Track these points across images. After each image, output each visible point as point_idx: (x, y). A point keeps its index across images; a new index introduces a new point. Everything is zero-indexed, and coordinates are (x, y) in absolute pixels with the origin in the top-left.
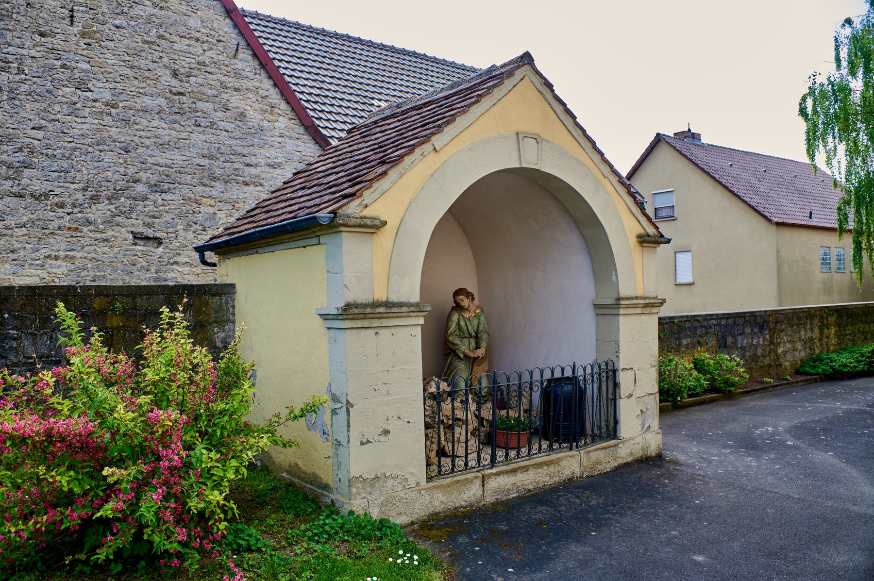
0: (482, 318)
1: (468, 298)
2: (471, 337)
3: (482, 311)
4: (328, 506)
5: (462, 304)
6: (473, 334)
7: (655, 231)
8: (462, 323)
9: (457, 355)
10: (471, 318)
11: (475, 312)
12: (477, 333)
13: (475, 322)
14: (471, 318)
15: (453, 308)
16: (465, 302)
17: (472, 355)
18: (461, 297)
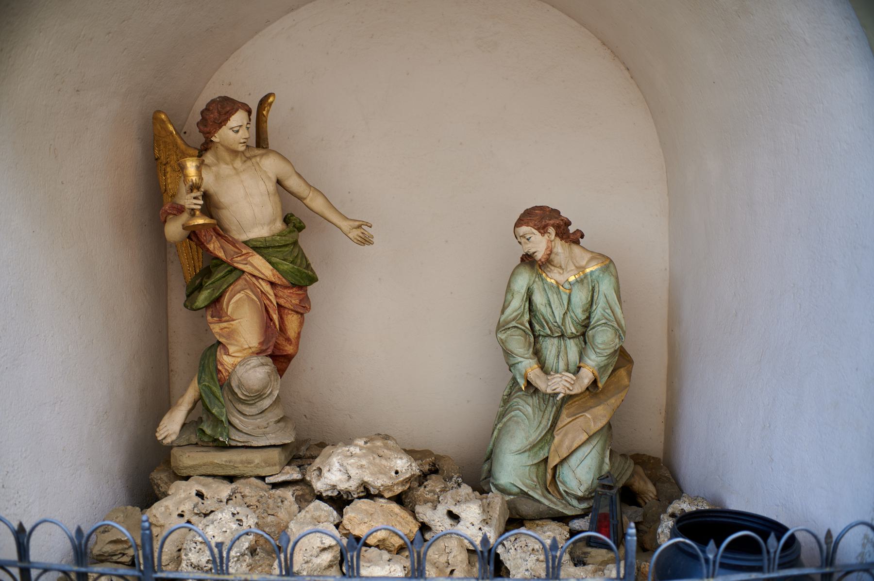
0: (606, 287)
8: (539, 299)
13: (580, 297)
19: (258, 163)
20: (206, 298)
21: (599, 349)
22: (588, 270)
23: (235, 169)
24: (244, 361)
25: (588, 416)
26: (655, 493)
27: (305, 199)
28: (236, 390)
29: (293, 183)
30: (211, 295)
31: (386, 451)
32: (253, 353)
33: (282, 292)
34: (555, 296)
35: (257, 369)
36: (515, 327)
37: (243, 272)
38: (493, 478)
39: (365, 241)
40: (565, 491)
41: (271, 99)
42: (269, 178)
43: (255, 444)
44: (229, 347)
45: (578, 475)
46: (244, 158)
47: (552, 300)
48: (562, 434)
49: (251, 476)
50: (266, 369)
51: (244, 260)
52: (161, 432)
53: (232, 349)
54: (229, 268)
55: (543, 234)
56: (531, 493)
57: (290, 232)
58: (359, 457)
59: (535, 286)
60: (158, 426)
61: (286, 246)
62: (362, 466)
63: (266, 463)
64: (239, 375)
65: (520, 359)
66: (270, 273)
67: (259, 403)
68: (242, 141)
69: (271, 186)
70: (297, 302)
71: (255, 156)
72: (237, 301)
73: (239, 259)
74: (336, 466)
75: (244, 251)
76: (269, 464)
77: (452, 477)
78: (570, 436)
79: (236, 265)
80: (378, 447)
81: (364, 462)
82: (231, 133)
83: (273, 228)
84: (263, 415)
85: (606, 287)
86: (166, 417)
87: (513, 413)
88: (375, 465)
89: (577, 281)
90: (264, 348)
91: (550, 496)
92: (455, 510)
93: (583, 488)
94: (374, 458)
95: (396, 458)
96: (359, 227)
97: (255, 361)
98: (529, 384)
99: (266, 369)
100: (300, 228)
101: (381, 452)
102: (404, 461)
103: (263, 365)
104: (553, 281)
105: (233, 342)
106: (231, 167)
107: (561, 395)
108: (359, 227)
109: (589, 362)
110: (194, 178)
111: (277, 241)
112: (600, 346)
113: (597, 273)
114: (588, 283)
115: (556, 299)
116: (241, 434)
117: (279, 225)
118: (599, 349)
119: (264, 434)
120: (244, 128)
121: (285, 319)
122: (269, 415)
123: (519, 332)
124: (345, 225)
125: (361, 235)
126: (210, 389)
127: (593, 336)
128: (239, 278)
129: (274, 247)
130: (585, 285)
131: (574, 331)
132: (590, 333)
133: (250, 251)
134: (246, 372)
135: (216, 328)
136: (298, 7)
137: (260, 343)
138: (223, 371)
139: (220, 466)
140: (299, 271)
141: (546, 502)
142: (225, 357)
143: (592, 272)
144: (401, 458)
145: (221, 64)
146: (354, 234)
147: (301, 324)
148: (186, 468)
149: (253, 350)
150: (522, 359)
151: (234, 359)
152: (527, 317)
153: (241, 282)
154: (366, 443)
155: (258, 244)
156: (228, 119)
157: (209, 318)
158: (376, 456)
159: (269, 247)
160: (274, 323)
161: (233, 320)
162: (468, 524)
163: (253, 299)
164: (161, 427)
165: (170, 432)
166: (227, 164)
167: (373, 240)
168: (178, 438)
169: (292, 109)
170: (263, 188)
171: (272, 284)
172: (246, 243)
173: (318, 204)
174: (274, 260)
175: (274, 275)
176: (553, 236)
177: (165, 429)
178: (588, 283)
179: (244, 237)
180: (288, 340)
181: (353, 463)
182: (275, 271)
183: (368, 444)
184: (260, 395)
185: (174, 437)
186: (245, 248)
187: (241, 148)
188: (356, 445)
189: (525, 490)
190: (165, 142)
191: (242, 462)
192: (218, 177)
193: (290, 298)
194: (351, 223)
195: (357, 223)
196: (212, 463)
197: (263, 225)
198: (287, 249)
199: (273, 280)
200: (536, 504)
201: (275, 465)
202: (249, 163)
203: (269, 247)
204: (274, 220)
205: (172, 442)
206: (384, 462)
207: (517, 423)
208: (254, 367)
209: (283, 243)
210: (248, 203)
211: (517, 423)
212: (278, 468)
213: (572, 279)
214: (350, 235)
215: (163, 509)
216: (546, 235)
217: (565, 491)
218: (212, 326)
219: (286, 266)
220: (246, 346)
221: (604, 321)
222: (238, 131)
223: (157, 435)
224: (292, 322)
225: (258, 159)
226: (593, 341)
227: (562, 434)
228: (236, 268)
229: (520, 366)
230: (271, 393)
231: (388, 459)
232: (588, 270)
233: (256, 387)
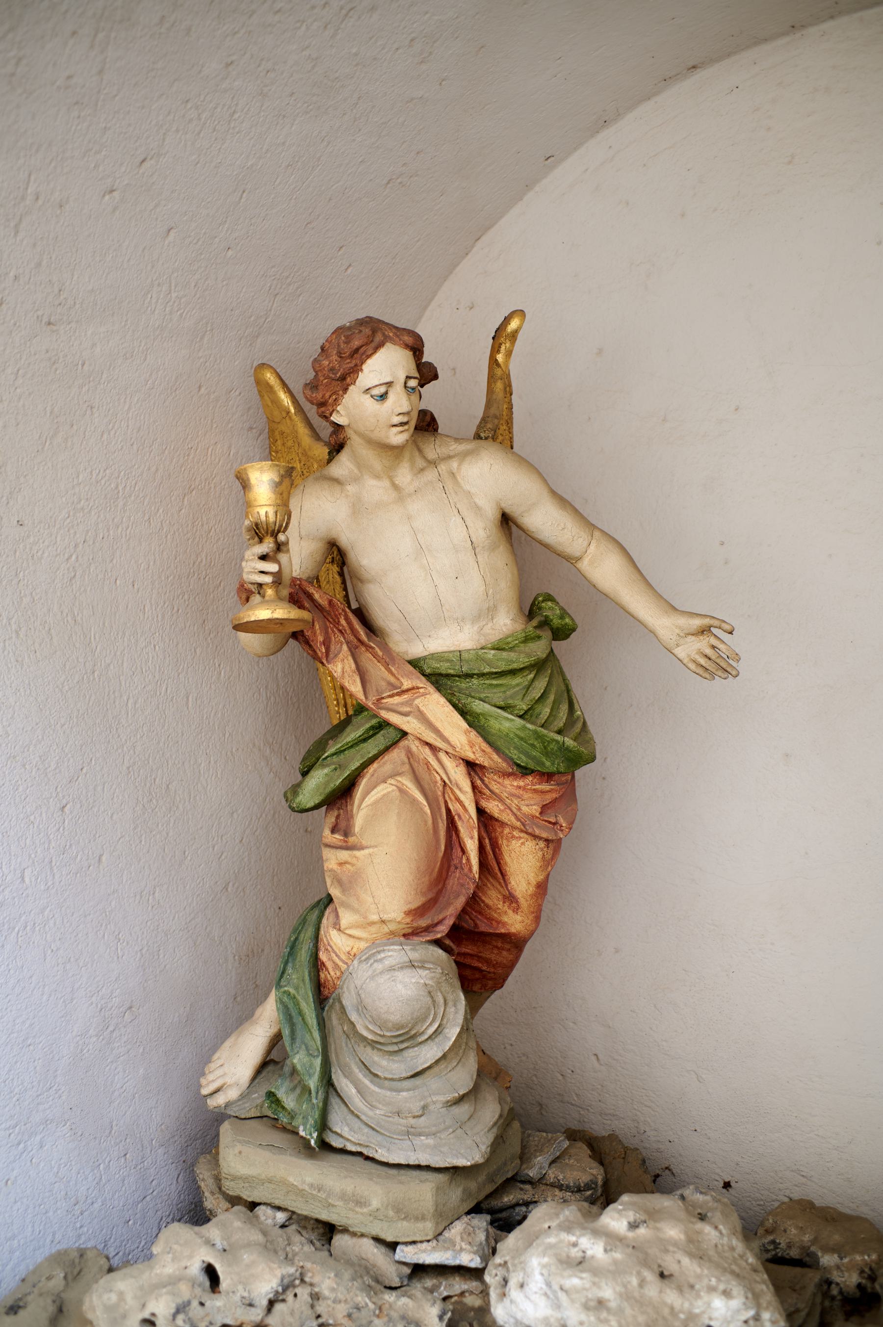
19: (453, 475)
20: (318, 787)
23: (396, 487)
24: (375, 948)
27: (579, 559)
28: (354, 1017)
29: (545, 521)
30: (329, 778)
31: (686, 1261)
32: (392, 933)
33: (495, 784)
35: (400, 975)
37: (404, 734)
39: (719, 667)
41: (514, 325)
42: (477, 509)
43: (381, 1155)
44: (341, 911)
46: (420, 463)
49: (363, 1235)
50: (422, 977)
51: (409, 703)
52: (211, 1077)
53: (346, 918)
54: (374, 722)
57: (526, 640)
58: (597, 1272)
60: (208, 1061)
61: (513, 672)
63: (398, 1211)
64: (358, 983)
66: (463, 739)
67: (410, 1053)
68: (397, 420)
69: (483, 528)
70: (535, 810)
71: (450, 457)
72: (376, 802)
73: (397, 700)
74: (537, 1282)
75: (407, 684)
76: (402, 1212)
79: (385, 714)
80: (665, 1245)
81: (608, 1292)
82: (369, 404)
83: (487, 629)
84: (417, 1081)
86: (228, 1044)
88: (640, 1303)
90: (423, 923)
94: (642, 1283)
95: (712, 1289)
96: (704, 631)
97: (395, 954)
99: (422, 977)
100: (561, 633)
101: (670, 1264)
102: (736, 1303)
103: (412, 965)
105: (352, 901)
106: (386, 483)
108: (704, 631)
110: (262, 512)
111: (489, 663)
116: (357, 1124)
117: (506, 622)
119: (410, 1133)
120: (399, 388)
121: (505, 849)
122: (431, 1082)
124: (665, 625)
125: (709, 651)
126: (297, 1004)
128: (395, 744)
129: (482, 675)
133: (421, 682)
134: (372, 978)
135: (332, 859)
136: (618, 115)
137: (408, 913)
138: (329, 965)
139: (301, 1193)
140: (538, 736)
142: (334, 933)
144: (727, 1294)
145: (454, 266)
146: (691, 649)
147: (547, 863)
148: (235, 1178)
149: (393, 927)
151: (351, 942)
153: (396, 755)
154: (633, 1226)
155: (444, 667)
156: (356, 370)
157: (327, 832)
158: (650, 1276)
159: (469, 676)
160: (468, 860)
161: (362, 848)
163: (414, 801)
164: (212, 1066)
165: (229, 1080)
166: (377, 477)
167: (741, 666)
168: (243, 1096)
169: (600, 352)
170: (458, 533)
171: (471, 766)
172: (415, 663)
173: (605, 570)
174: (478, 706)
175: (472, 745)
177: (219, 1072)
179: (417, 650)
180: (510, 898)
181: (577, 1291)
182: (473, 734)
183: (642, 1231)
184: (407, 1037)
185: (233, 1094)
186: (408, 676)
187: (398, 437)
190: (282, 433)
191: (343, 1196)
192: (357, 509)
193: (517, 800)
194: (683, 621)
195: (697, 623)
196: (284, 1182)
197: (461, 621)
198: (517, 680)
199: (471, 756)
201: (423, 1218)
202: (431, 475)
203: (469, 676)
204: (491, 612)
205: (228, 1105)
206: (672, 1297)
208: (391, 969)
209: (503, 667)
210: (433, 569)
212: (428, 1227)
214: (677, 651)
215: (114, 1297)
218: (327, 853)
219: (506, 724)
220: (375, 918)
222: (383, 397)
223: (203, 1081)
224: (522, 861)
225: (454, 464)
228: (383, 725)
230: (437, 1032)
231: (687, 1288)
233: (395, 1018)
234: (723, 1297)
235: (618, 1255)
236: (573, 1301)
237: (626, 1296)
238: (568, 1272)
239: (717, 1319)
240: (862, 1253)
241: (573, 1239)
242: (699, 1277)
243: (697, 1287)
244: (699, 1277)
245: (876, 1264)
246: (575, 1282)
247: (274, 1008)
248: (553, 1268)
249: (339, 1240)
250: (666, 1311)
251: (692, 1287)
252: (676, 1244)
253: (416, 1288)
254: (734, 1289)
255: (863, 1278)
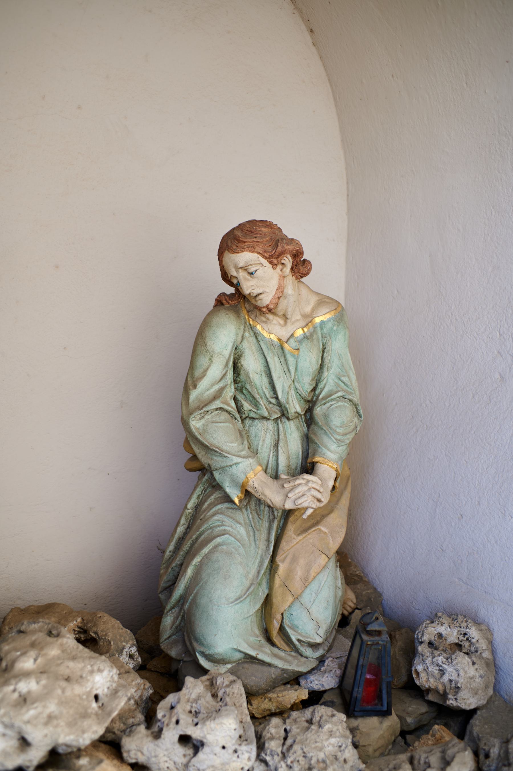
0: (339, 345)
1: (274, 258)
2: (284, 414)
3: (341, 316)
4: (337, 388)
5: (249, 287)
6: (296, 407)
7: (239, 342)
8: (251, 364)
9: (217, 487)
10: (290, 341)
11: (308, 319)
12: (310, 404)
13: (309, 360)
14: (290, 341)
15: (221, 302)
16: (263, 279)
17: (273, 494)
18: (245, 257)
21: (338, 434)
22: (317, 320)
25: (324, 529)
26: (355, 601)
31: (71, 664)
34: (276, 359)
36: (221, 409)
38: (202, 644)
40: (299, 640)
45: (314, 615)
47: (272, 366)
48: (288, 560)
55: (273, 265)
56: (260, 657)
59: (245, 345)
62: (50, 718)
65: (236, 460)
77: (124, 648)
78: (302, 561)
85: (339, 345)
87: (218, 540)
89: (305, 337)
91: (275, 650)
92: (195, 733)
93: (322, 632)
95: (92, 672)
98: (247, 494)
104: (272, 337)
107: (310, 512)
109: (329, 454)
112: (339, 430)
113: (330, 325)
114: (318, 339)
115: (278, 365)
118: (338, 434)
123: (224, 416)
127: (326, 416)
130: (315, 341)
131: (299, 410)
132: (318, 411)
141: (279, 663)
143: (322, 322)
144: (100, 671)
150: (239, 460)
152: (230, 392)
162: (218, 750)
176: (287, 270)
178: (318, 339)
181: (36, 717)
183: (39, 660)
188: (26, 674)
189: (253, 653)
200: (265, 668)
207: (229, 554)
211: (229, 554)
213: (299, 333)
216: (280, 267)
217: (299, 640)
221: (340, 394)
226: (327, 424)
227: (288, 560)
229: (234, 470)
232: (317, 320)
234: (99, 673)
235: (43, 682)
236: (35, 726)
237: (61, 703)
238: (24, 709)
239: (99, 688)
240: (72, 621)
241: (11, 688)
242: (82, 669)
243: (84, 675)
244: (82, 669)
245: (81, 623)
246: (32, 712)
247: (174, 594)
248: (12, 713)
249: (173, 705)
250: (78, 699)
251: (81, 677)
252: (59, 658)
253: (62, 750)
254: (100, 666)
255: (76, 634)
